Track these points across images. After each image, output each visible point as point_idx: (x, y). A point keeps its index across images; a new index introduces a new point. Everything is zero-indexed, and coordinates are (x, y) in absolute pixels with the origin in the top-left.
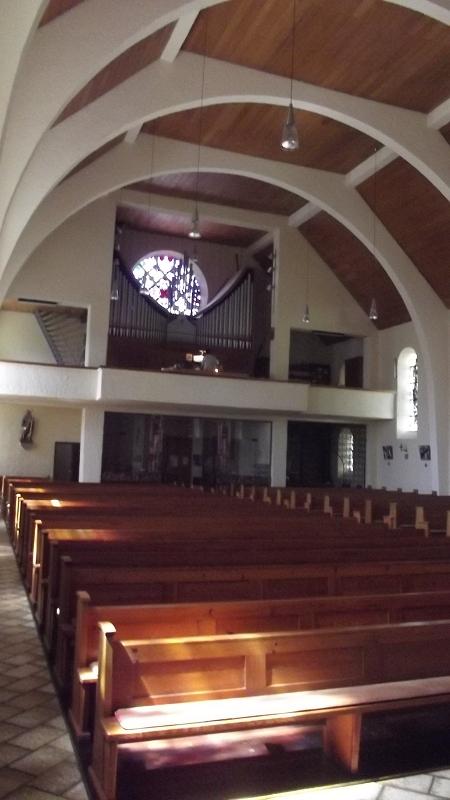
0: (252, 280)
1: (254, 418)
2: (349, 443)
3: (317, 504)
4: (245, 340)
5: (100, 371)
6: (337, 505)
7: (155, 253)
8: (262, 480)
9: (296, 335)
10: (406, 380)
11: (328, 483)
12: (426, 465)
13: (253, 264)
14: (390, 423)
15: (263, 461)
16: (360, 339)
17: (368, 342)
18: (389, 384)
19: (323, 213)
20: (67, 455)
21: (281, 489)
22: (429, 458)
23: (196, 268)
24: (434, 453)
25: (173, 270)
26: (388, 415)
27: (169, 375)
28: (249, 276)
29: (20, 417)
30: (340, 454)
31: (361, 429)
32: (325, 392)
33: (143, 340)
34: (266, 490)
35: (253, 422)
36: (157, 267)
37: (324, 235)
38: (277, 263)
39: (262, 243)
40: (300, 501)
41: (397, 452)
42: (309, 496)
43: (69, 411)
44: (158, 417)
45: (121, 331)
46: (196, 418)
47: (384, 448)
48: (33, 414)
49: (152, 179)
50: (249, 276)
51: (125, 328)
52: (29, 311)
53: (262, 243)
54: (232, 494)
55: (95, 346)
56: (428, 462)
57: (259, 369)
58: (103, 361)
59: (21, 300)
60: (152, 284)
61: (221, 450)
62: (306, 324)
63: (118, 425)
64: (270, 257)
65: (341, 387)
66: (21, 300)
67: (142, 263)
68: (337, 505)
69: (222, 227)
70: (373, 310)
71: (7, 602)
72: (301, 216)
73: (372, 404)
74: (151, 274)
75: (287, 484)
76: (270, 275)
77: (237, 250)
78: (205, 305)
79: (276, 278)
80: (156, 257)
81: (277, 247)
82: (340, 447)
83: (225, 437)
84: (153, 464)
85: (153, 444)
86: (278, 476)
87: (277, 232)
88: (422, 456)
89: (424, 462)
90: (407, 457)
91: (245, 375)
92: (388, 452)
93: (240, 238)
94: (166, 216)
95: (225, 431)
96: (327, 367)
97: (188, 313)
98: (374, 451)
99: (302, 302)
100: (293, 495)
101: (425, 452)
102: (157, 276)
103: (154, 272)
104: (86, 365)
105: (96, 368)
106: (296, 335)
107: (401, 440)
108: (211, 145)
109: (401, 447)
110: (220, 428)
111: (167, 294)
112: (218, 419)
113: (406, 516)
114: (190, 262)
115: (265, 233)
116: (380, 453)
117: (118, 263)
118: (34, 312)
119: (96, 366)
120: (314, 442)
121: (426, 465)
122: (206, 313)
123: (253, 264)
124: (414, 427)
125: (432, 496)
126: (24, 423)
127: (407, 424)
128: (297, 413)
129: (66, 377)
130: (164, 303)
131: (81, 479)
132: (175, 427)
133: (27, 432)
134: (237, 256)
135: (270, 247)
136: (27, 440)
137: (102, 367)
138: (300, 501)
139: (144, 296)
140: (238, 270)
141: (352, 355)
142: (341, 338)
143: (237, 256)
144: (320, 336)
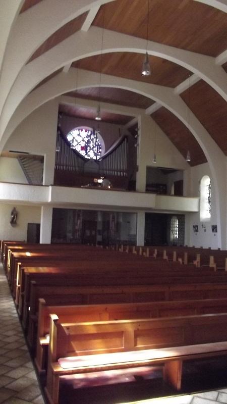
0: (127, 141)
1: (128, 211)
2: (176, 224)
3: (160, 255)
4: (123, 172)
5: (50, 187)
6: (170, 255)
7: (78, 128)
8: (132, 242)
9: (149, 169)
10: (205, 192)
11: (166, 244)
12: (215, 235)
13: (128, 133)
14: (197, 214)
15: (133, 233)
16: (182, 171)
17: (186, 173)
18: (196, 194)
19: (163, 108)
20: (34, 230)
21: (142, 247)
22: (216, 231)
23: (99, 135)
24: (219, 229)
25: (87, 137)
26: (196, 210)
27: (85, 189)
28: (126, 139)
29: (10, 211)
30: (171, 229)
31: (182, 217)
32: (164, 198)
33: (72, 172)
34: (134, 248)
35: (127, 213)
36: (79, 135)
37: (163, 119)
38: (140, 133)
39: (132, 123)
40: (151, 253)
41: (200, 228)
42: (156, 251)
43: (35, 207)
44: (80, 211)
45: (61, 167)
46: (99, 211)
47: (194, 226)
48: (16, 209)
49: (76, 90)
50: (126, 139)
51: (63, 166)
52: (14, 157)
53: (132, 123)
54: (117, 250)
55: (48, 175)
56: (216, 233)
57: (131, 186)
58: (52, 182)
59: (10, 151)
60: (77, 143)
61: (112, 227)
62: (154, 164)
63: (59, 215)
64: (136, 130)
65: (172, 196)
66: (10, 151)
67: (71, 133)
68: (170, 255)
69: (112, 114)
70: (188, 157)
71: (3, 304)
72: (152, 109)
73: (188, 204)
74: (76, 138)
75: (145, 245)
76: (136, 139)
77: (120, 126)
78: (104, 154)
79: (139, 141)
80: (79, 130)
81: (140, 125)
82: (171, 226)
83: (113, 221)
84: (77, 234)
85: (77, 224)
86: (140, 241)
87: (140, 117)
88: (213, 230)
89: (214, 233)
90: (205, 231)
91: (124, 189)
92: (196, 228)
93: (121, 120)
94: (84, 109)
95: (114, 218)
96: (165, 185)
97: (95, 158)
98: (189, 228)
99: (152, 152)
100: (148, 250)
101: (214, 228)
102: (79, 139)
103: (78, 137)
104: (43, 184)
105: (48, 186)
106: (149, 169)
107: (202, 222)
108: (107, 73)
109: (202, 226)
110: (111, 216)
111: (84, 148)
112: (110, 212)
113: (205, 260)
114: (96, 132)
115: (134, 118)
116: (192, 229)
117: (59, 133)
118: (17, 158)
119: (48, 185)
120: (158, 223)
121: (215, 235)
122: (104, 158)
123: (128, 133)
124: (209, 216)
125: (218, 250)
126: (12, 214)
127: (205, 214)
128: (150, 209)
129: (33, 190)
130: (83, 153)
131: (41, 242)
132: (89, 215)
133: (14, 218)
134: (119, 129)
135: (136, 125)
136: (14, 222)
137: (51, 185)
138: (151, 253)
139: (72, 149)
140: (120, 136)
141: (178, 179)
142: (172, 171)
143: (119, 129)
144: (161, 170)
